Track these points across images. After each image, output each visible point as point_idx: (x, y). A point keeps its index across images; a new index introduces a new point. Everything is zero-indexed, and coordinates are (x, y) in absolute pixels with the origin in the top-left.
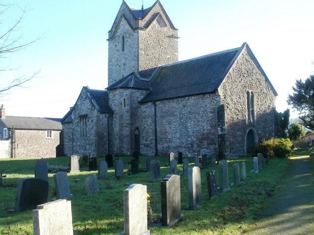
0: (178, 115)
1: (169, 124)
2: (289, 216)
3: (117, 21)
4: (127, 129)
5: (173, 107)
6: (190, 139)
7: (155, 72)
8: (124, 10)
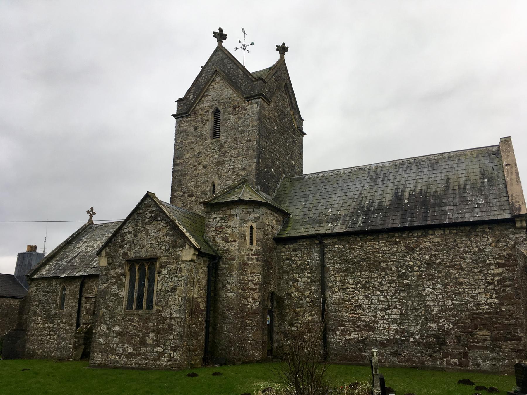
0: (394, 269)
1: (365, 287)
3: (202, 81)
4: (256, 295)
5: (375, 251)
6: (433, 325)
7: (302, 176)
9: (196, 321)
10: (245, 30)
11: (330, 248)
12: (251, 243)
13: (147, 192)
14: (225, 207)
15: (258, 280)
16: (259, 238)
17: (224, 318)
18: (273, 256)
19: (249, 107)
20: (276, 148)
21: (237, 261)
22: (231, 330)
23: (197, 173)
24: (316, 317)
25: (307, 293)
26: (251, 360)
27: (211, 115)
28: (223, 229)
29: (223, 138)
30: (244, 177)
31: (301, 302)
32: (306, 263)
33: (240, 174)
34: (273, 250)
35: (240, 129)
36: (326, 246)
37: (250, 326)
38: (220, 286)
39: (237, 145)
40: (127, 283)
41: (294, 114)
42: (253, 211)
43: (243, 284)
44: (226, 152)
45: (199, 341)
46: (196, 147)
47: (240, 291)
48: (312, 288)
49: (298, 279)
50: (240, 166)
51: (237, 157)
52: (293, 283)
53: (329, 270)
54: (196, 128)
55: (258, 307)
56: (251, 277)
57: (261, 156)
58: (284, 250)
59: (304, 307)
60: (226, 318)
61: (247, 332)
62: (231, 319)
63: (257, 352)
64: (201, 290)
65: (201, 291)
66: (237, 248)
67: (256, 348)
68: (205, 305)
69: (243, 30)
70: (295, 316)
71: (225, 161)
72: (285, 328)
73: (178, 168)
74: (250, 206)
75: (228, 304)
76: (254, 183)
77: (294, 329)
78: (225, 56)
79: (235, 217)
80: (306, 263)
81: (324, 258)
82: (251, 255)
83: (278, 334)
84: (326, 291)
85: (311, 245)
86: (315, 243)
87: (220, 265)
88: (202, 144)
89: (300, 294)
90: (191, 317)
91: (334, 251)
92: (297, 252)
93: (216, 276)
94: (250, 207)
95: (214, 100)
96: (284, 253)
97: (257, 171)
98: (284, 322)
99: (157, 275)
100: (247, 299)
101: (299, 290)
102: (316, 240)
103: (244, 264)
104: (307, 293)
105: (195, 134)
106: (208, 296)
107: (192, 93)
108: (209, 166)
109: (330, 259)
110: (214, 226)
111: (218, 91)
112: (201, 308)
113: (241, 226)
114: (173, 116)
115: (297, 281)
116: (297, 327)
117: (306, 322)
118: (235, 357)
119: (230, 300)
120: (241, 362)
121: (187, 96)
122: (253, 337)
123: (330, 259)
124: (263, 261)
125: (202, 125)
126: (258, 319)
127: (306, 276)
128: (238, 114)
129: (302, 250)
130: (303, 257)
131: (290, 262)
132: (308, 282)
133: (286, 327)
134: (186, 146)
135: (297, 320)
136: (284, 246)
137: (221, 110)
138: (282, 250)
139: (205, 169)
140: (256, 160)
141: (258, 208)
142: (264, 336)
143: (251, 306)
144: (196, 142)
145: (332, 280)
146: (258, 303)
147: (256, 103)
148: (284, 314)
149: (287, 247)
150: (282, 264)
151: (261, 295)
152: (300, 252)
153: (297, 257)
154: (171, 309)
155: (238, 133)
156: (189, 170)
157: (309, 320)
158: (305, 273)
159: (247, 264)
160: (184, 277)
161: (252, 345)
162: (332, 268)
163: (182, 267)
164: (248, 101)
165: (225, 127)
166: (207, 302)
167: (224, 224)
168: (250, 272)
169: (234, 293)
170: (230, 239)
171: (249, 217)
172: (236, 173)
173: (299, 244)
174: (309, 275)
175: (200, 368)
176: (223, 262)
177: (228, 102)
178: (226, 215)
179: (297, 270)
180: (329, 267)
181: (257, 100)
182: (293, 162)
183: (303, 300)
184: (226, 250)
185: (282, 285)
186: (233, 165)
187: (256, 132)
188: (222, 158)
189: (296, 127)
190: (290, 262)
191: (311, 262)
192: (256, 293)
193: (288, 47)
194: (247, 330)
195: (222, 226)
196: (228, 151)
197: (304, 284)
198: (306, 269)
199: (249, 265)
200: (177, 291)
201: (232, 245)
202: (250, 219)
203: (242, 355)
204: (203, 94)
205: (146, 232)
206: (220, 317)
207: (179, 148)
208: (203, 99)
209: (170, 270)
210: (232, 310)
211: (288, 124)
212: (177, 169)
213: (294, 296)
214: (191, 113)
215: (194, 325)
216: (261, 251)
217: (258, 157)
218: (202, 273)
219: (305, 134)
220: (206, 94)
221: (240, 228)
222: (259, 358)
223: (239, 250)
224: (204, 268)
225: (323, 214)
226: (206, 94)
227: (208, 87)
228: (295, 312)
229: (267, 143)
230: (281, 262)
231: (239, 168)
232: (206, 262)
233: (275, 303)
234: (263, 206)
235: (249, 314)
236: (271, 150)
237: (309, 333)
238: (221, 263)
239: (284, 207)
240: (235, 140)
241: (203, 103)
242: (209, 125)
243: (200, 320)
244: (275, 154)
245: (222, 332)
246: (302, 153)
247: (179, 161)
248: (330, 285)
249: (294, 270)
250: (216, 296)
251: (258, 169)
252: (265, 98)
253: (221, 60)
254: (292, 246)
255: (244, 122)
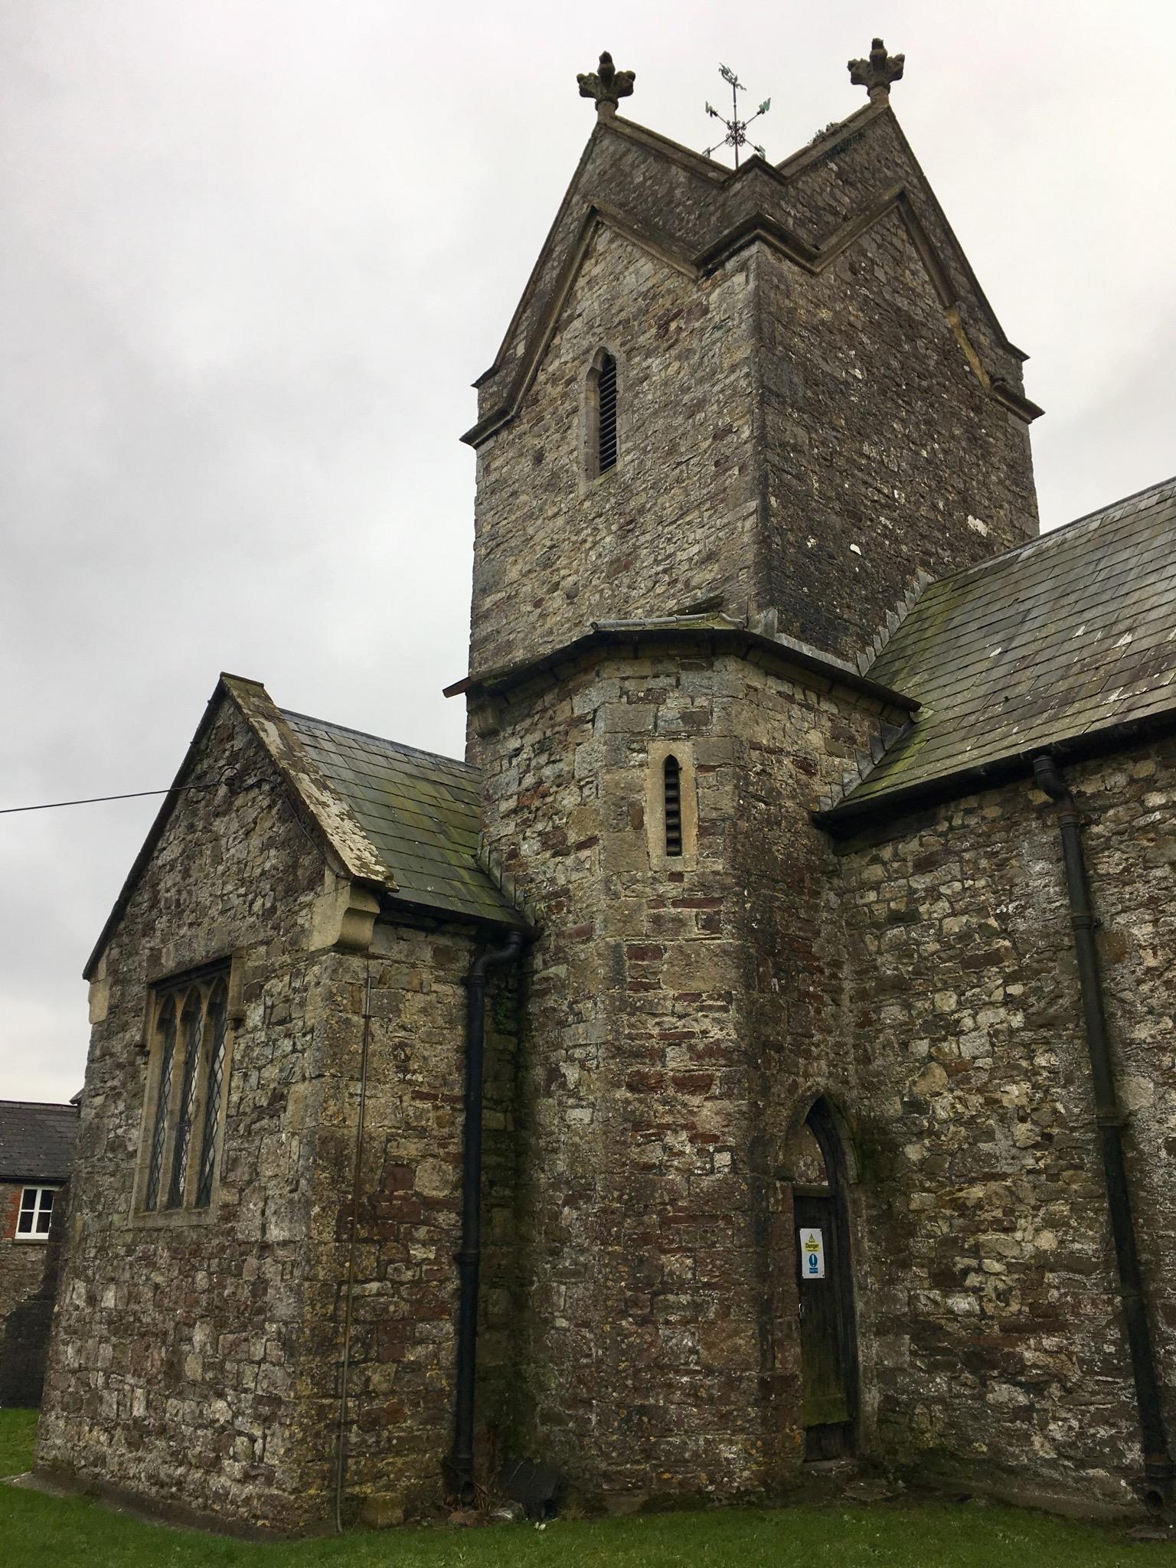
2: (100, 1460)
3: (550, 275)
4: (708, 1112)
8: (615, 175)
9: (391, 1262)
10: (735, 72)
11: (1117, 821)
12: (674, 845)
13: (223, 675)
14: (550, 689)
15: (716, 1033)
16: (714, 815)
17: (559, 1239)
18: (816, 908)
19: (714, 297)
20: (868, 457)
21: (605, 937)
22: (586, 1310)
23: (547, 627)
24: (1083, 1236)
25: (1015, 1093)
26: (700, 1491)
27: (584, 388)
28: (544, 796)
29: (628, 458)
30: (711, 590)
31: (985, 1147)
32: (993, 922)
33: (693, 583)
34: (817, 881)
35: (686, 398)
36: (1095, 810)
37: (681, 1286)
38: (539, 1073)
39: (677, 471)
40: (151, 1088)
41: (964, 325)
42: (678, 681)
43: (638, 1054)
44: (641, 511)
45: (416, 1367)
46: (540, 528)
47: (622, 1093)
48: (1041, 1061)
49: (958, 1021)
50: (696, 549)
51: (681, 517)
52: (934, 1042)
53: (1124, 949)
54: (539, 458)
55: (725, 1179)
56: (680, 1017)
57: (772, 480)
58: (877, 872)
59: (1004, 1176)
60: (563, 1243)
61: (667, 1322)
62: (582, 1250)
63: (731, 1443)
64: (418, 1096)
65: (418, 1103)
66: (600, 873)
67: (724, 1417)
68: (451, 1172)
69: (725, 72)
70: (962, 1230)
71: (639, 547)
72: (913, 1300)
73: (487, 628)
74: (660, 662)
75: (571, 1166)
76: (753, 605)
77: (961, 1303)
78: (623, 146)
79: (590, 725)
80: (993, 922)
81: (1086, 882)
82: (675, 904)
83: (881, 1331)
84: (1123, 1073)
85: (1011, 824)
86: (1028, 807)
87: (536, 972)
88: (560, 510)
89: (977, 1100)
90: (350, 1240)
91: (1144, 829)
92: (940, 873)
93: (520, 1026)
94: (660, 668)
95: (592, 327)
96: (876, 886)
97: (760, 549)
98: (905, 1265)
99: (233, 1034)
100: (659, 1137)
101: (967, 1080)
102: (1035, 786)
103: (638, 953)
104: (1015, 1093)
105: (536, 483)
106: (473, 1131)
107: (522, 332)
108: (585, 586)
109: (1124, 878)
110: (514, 788)
111: (605, 287)
112: (427, 1192)
113: (615, 762)
114: (467, 439)
115: (955, 1030)
116: (976, 1291)
117: (1027, 1267)
118: (603, 1466)
119: (576, 1145)
120: (641, 1498)
121: (508, 349)
122: (704, 1353)
123: (1124, 878)
124: (743, 927)
125: (557, 436)
126: (729, 1251)
127: (998, 996)
128: (677, 341)
129: (967, 856)
130: (974, 892)
131: (908, 933)
132: (1012, 1032)
133: (917, 1297)
134: (510, 536)
135: (976, 1251)
136: (874, 852)
137: (617, 355)
138: (865, 876)
139: (571, 603)
140: (753, 505)
141: (699, 668)
142: (768, 1348)
143: (687, 1172)
144: (541, 510)
145: (1154, 1002)
146: (724, 1159)
147: (743, 267)
148: (905, 1217)
149: (887, 853)
150: (873, 948)
151: (740, 1112)
152: (955, 868)
153: (939, 897)
154: (266, 1200)
155: (680, 419)
156: (522, 625)
157: (1040, 1254)
158: (993, 979)
159: (657, 952)
160: (312, 1031)
161: (698, 1402)
162: (1142, 932)
163: (309, 983)
164: (709, 274)
165: (634, 412)
166: (470, 1161)
167: (547, 772)
168: (672, 993)
169: (593, 1105)
170: (573, 837)
171: (656, 717)
172: (680, 586)
173: (943, 827)
174: (1016, 989)
175: (390, 1526)
176: (547, 956)
177: (640, 310)
178: (553, 726)
179: (949, 970)
180: (1127, 925)
181: (745, 254)
182: (976, 524)
183: (998, 1135)
184: (556, 895)
185: (880, 1062)
186: (670, 556)
187: (749, 385)
188: (627, 542)
189: (986, 380)
190: (908, 933)
191: (1020, 912)
192: (709, 1104)
193: (901, 59)
194: (668, 1308)
195: (540, 782)
196: (648, 506)
197: (993, 1045)
198: (995, 958)
199: (666, 956)
200: (290, 1108)
201: (579, 866)
202: (661, 723)
203: (648, 1454)
204: (557, 322)
205: (213, 848)
206: (540, 1239)
207: (488, 554)
208: (557, 341)
209: (273, 1006)
210: (589, 1199)
211: (932, 363)
212: (484, 634)
213: (942, 1114)
214: (520, 408)
215: (374, 1286)
216: (730, 881)
217: (762, 488)
218: (424, 1011)
219: (1036, 412)
220: (565, 315)
221: (608, 777)
222: (743, 1475)
223: (607, 881)
224: (435, 987)
225: (1084, 666)
226: (565, 315)
227: (571, 287)
228: (961, 1207)
229: (808, 429)
230: (868, 938)
231: (690, 559)
232: (454, 959)
233: (851, 1159)
234: (726, 654)
235: (676, 1220)
236: (840, 462)
237: (1050, 1331)
238: (538, 962)
239: (906, 687)
240: (673, 450)
241: (557, 356)
242: (582, 430)
243: (417, 1252)
244: (865, 483)
245: (548, 1322)
246: (1032, 491)
247: (488, 600)
248: (1143, 1033)
249: (934, 968)
250: (525, 1128)
251: (763, 540)
252: (783, 235)
253: (612, 166)
254: (914, 845)
255: (701, 363)
